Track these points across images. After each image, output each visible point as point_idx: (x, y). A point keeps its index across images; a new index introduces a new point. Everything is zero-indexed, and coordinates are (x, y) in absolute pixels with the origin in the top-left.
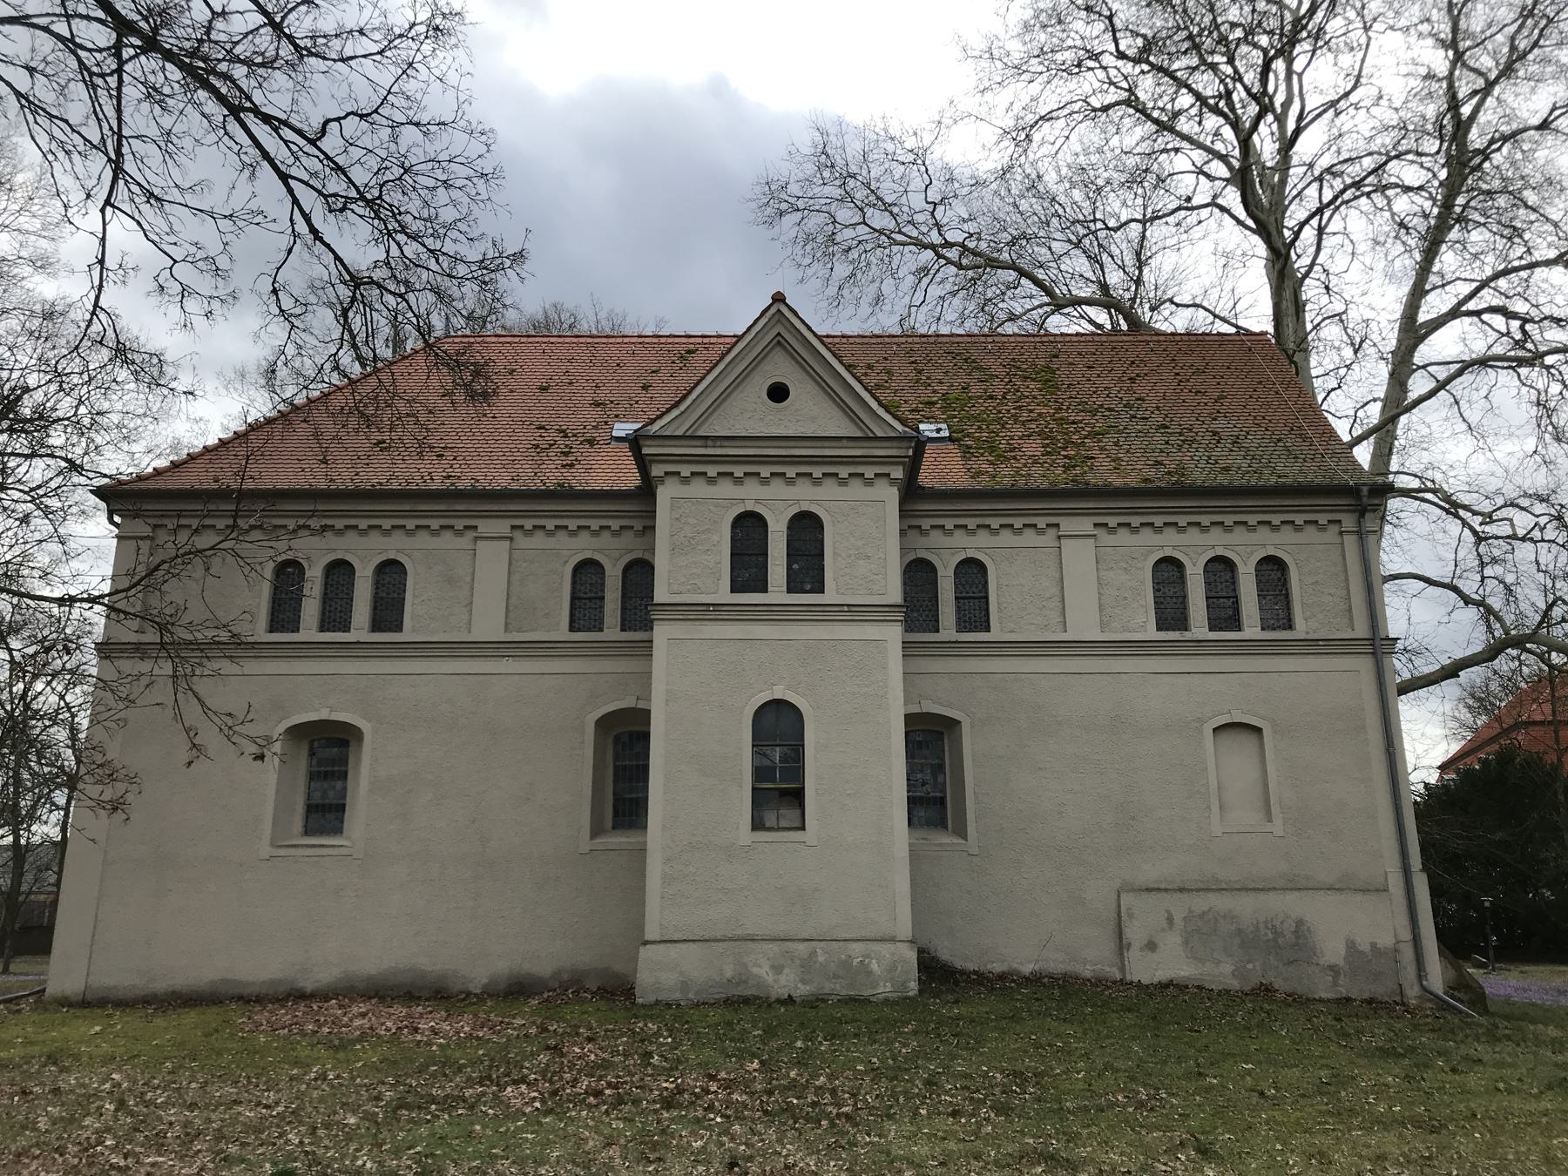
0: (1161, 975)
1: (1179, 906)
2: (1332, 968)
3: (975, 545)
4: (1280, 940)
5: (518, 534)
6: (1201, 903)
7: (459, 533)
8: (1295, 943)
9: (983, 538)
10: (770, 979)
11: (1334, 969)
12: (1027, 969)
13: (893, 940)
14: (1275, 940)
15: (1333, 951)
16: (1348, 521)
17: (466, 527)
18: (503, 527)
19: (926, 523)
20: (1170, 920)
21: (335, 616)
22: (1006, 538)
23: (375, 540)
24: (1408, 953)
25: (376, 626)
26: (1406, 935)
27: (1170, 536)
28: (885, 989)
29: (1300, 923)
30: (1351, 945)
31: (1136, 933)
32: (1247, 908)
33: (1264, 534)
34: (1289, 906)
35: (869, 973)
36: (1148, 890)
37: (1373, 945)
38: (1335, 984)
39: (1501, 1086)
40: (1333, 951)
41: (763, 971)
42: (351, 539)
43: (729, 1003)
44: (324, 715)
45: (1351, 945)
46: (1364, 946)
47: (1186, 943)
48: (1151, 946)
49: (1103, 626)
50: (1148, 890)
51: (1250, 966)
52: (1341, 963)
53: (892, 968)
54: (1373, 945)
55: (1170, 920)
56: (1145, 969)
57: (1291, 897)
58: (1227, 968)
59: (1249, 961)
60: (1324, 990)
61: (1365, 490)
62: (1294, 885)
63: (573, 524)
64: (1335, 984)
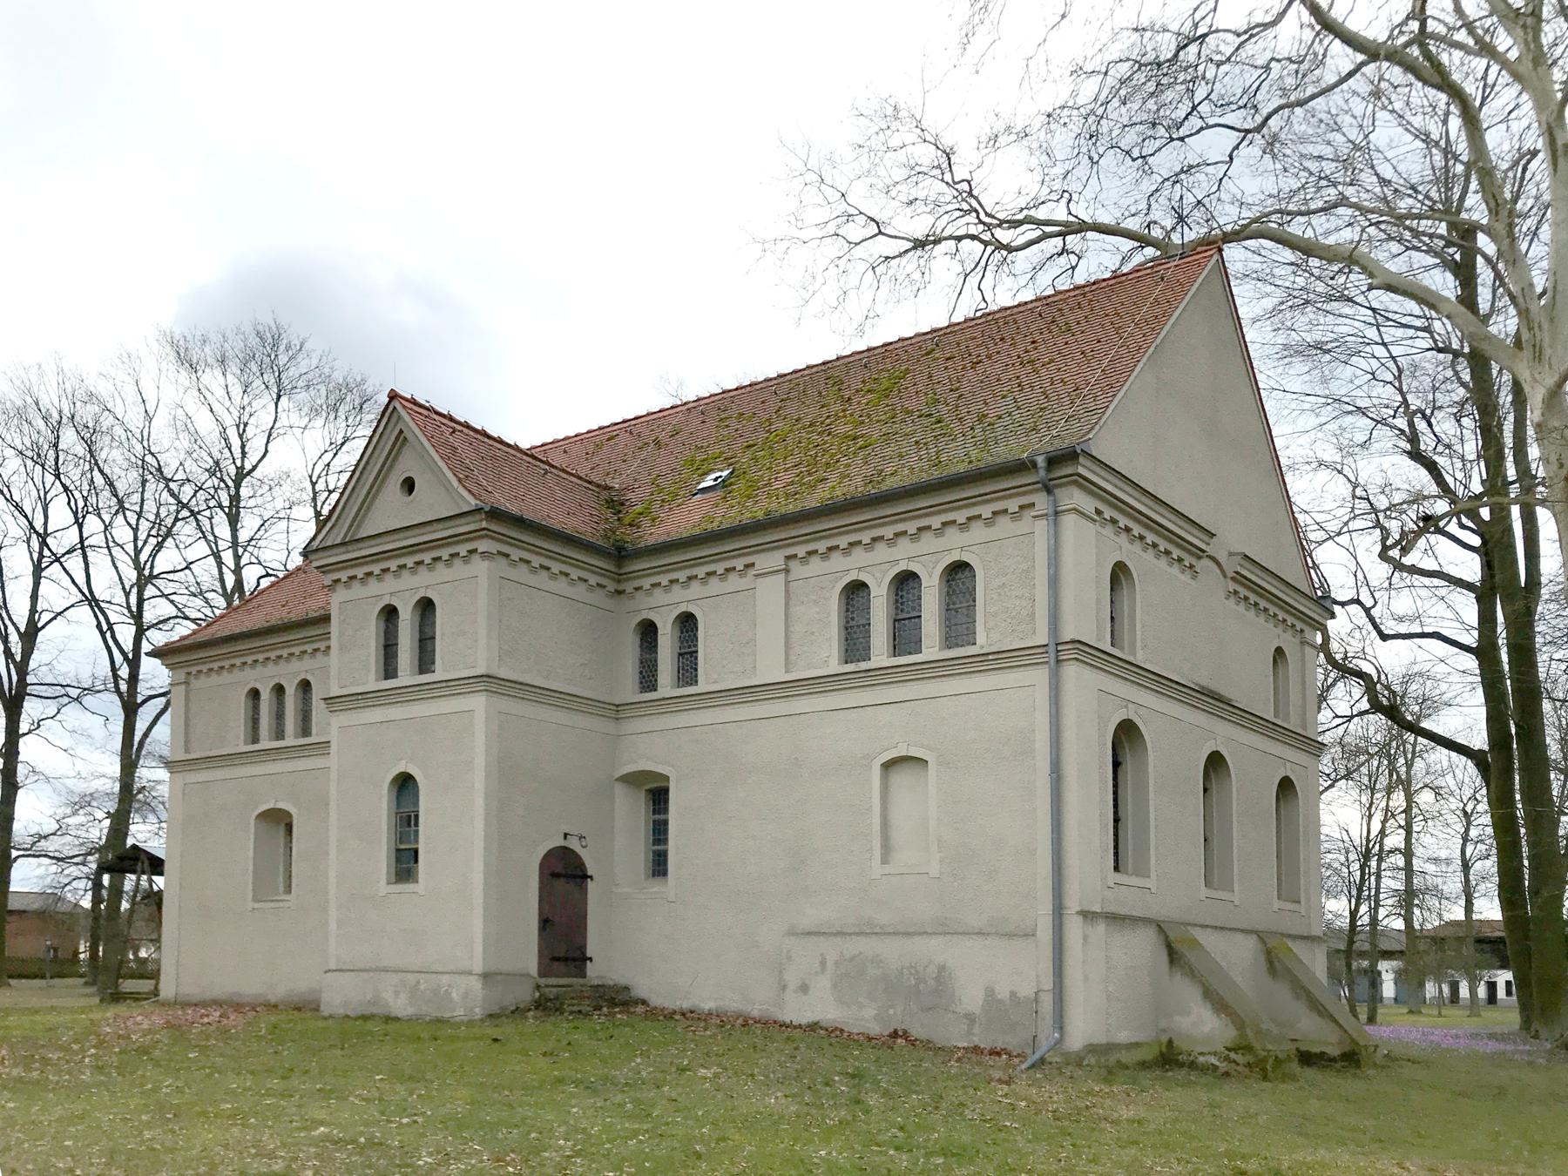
0: (805, 1018)
1: (831, 949)
2: (967, 1016)
3: (954, 546)
4: (921, 986)
5: (793, 564)
6: (851, 947)
7: (1016, 516)
8: (935, 989)
9: (696, 589)
10: (391, 1001)
11: (970, 1018)
12: (708, 1005)
13: (470, 973)
14: (916, 985)
15: (971, 998)
16: (1041, 501)
17: (1022, 507)
18: (775, 559)
19: (646, 583)
20: (823, 963)
21: (905, 636)
22: (715, 586)
23: (882, 552)
24: (1047, 1001)
25: (896, 650)
26: (1048, 984)
27: (953, 537)
28: (459, 1013)
29: (942, 968)
30: (990, 992)
31: (792, 978)
32: (893, 952)
33: (837, 561)
34: (935, 950)
35: (451, 1000)
36: (809, 933)
37: (1013, 994)
38: (970, 1032)
39: (75, 1047)
40: (971, 998)
41: (388, 995)
42: (859, 557)
43: (365, 1018)
44: (270, 805)
45: (990, 992)
46: (1003, 993)
47: (835, 986)
48: (804, 988)
49: (187, 751)
50: (809, 933)
51: (891, 1012)
52: (978, 1011)
53: (466, 996)
54: (1013, 994)
55: (823, 963)
56: (798, 1011)
57: (936, 942)
58: (870, 1012)
59: (891, 1007)
60: (958, 1038)
61: (1041, 461)
62: (945, 929)
63: (961, 517)
64: (970, 1032)
